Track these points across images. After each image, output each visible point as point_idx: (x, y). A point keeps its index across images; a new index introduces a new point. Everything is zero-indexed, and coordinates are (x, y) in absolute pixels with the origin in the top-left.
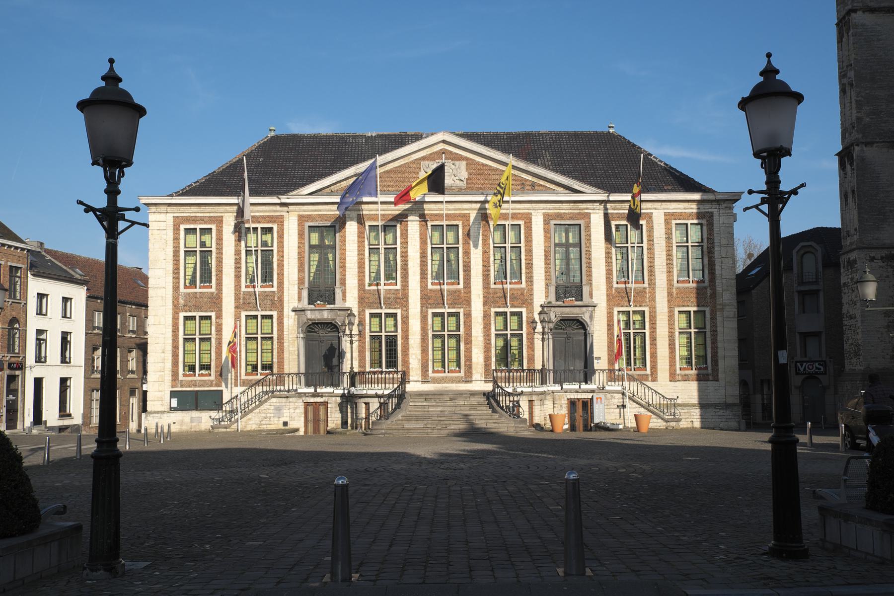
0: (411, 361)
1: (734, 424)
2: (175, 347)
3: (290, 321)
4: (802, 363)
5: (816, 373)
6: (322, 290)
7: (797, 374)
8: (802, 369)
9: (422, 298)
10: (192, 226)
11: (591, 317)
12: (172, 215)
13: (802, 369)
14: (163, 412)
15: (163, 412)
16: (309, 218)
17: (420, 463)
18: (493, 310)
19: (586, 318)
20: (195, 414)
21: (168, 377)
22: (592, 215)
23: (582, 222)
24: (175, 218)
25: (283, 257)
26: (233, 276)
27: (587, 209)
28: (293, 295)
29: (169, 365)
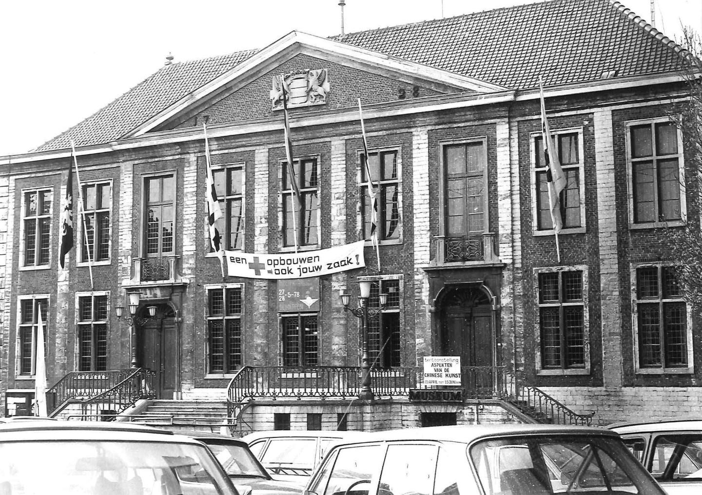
22: (498, 127)
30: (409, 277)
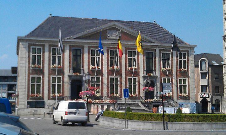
0: (104, 92)
1: (81, 125)
2: (28, 87)
3: (66, 79)
4: (202, 94)
5: (206, 97)
6: (76, 68)
7: (200, 97)
8: (202, 96)
9: (107, 73)
10: (35, 47)
11: (156, 80)
13: (202, 96)
14: (24, 109)
15: (24, 109)
16: (73, 46)
17: (173, 116)
18: (128, 77)
19: (154, 80)
20: (35, 109)
21: (26, 97)
23: (153, 52)
24: (29, 44)
26: (48, 64)
27: (155, 48)
28: (67, 71)
29: (26, 93)
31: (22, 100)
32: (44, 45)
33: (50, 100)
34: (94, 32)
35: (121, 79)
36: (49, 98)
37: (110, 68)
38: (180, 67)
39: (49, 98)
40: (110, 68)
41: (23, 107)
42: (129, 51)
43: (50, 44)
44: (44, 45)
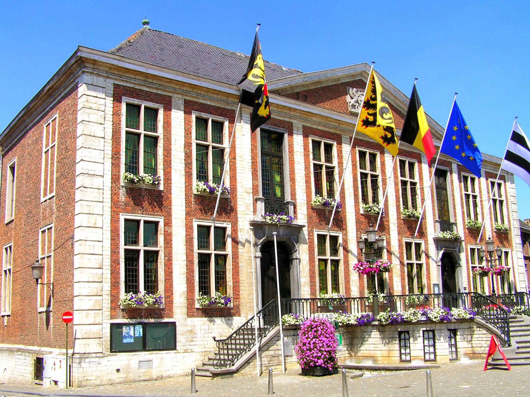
2: (115, 262)
3: (245, 233)
12: (112, 81)
18: (405, 240)
25: (235, 159)
26: (183, 173)
28: (248, 210)
30: (426, 243)
31: (92, 317)
32: (170, 97)
33: (193, 316)
34: (312, 84)
35: (168, 223)
36: (191, 312)
37: (197, 186)
38: (132, 167)
39: (191, 312)
40: (197, 186)
41: (93, 346)
42: (128, 104)
43: (188, 98)
44: (170, 97)
